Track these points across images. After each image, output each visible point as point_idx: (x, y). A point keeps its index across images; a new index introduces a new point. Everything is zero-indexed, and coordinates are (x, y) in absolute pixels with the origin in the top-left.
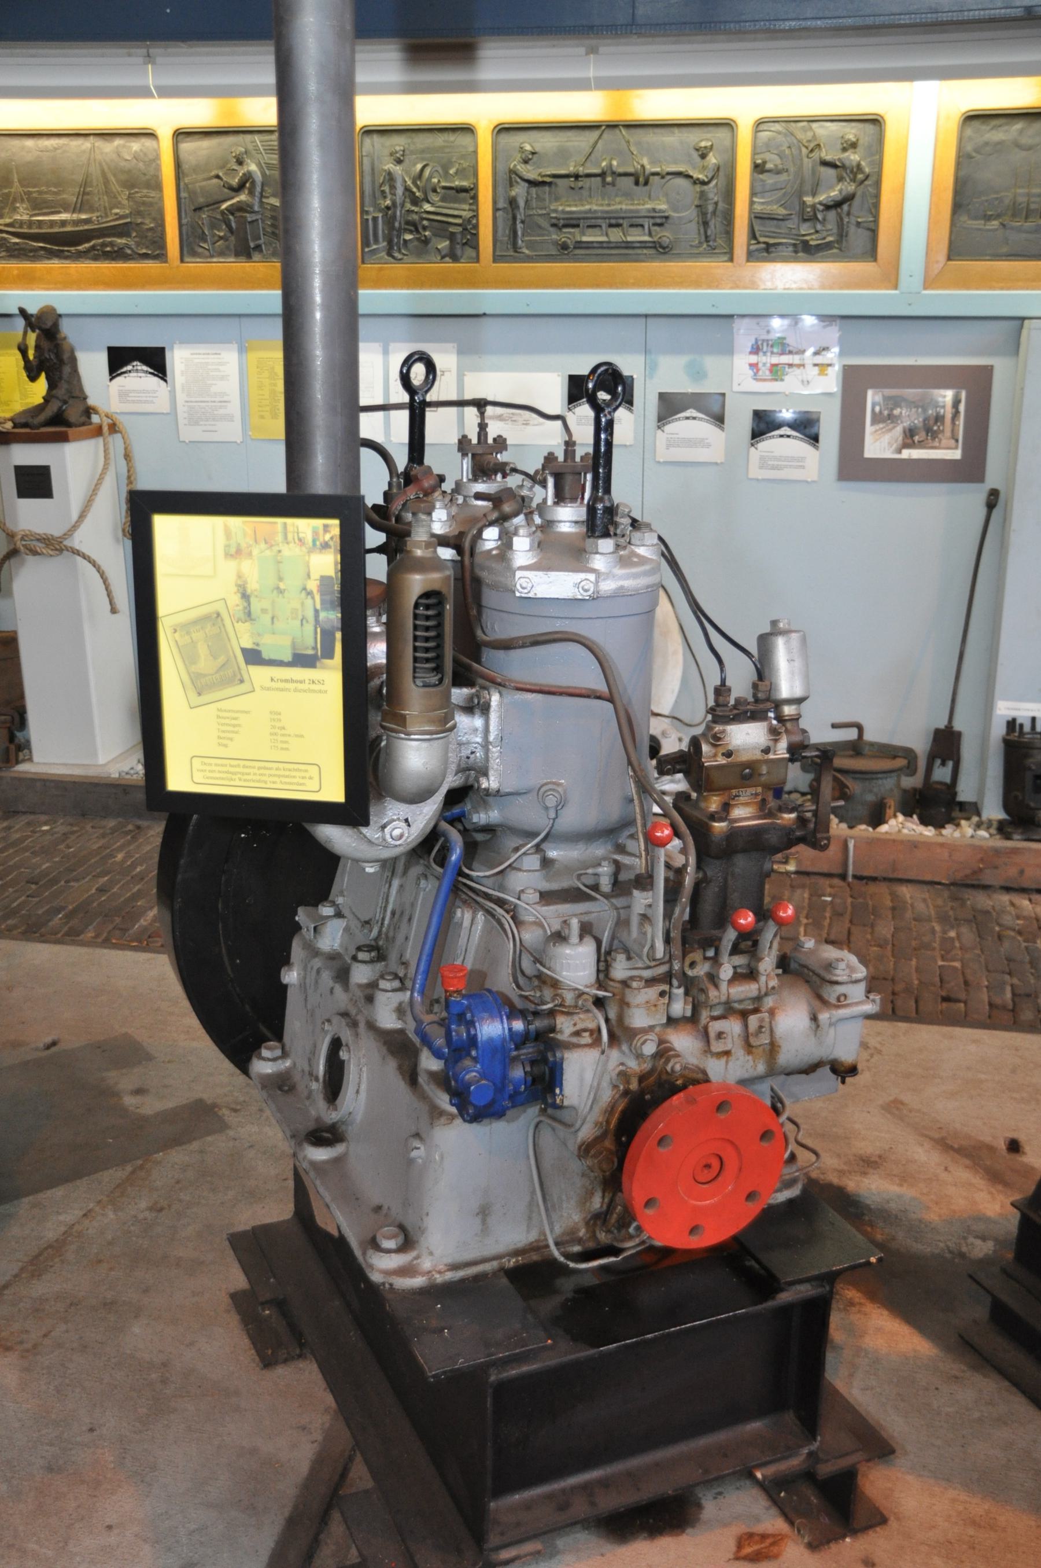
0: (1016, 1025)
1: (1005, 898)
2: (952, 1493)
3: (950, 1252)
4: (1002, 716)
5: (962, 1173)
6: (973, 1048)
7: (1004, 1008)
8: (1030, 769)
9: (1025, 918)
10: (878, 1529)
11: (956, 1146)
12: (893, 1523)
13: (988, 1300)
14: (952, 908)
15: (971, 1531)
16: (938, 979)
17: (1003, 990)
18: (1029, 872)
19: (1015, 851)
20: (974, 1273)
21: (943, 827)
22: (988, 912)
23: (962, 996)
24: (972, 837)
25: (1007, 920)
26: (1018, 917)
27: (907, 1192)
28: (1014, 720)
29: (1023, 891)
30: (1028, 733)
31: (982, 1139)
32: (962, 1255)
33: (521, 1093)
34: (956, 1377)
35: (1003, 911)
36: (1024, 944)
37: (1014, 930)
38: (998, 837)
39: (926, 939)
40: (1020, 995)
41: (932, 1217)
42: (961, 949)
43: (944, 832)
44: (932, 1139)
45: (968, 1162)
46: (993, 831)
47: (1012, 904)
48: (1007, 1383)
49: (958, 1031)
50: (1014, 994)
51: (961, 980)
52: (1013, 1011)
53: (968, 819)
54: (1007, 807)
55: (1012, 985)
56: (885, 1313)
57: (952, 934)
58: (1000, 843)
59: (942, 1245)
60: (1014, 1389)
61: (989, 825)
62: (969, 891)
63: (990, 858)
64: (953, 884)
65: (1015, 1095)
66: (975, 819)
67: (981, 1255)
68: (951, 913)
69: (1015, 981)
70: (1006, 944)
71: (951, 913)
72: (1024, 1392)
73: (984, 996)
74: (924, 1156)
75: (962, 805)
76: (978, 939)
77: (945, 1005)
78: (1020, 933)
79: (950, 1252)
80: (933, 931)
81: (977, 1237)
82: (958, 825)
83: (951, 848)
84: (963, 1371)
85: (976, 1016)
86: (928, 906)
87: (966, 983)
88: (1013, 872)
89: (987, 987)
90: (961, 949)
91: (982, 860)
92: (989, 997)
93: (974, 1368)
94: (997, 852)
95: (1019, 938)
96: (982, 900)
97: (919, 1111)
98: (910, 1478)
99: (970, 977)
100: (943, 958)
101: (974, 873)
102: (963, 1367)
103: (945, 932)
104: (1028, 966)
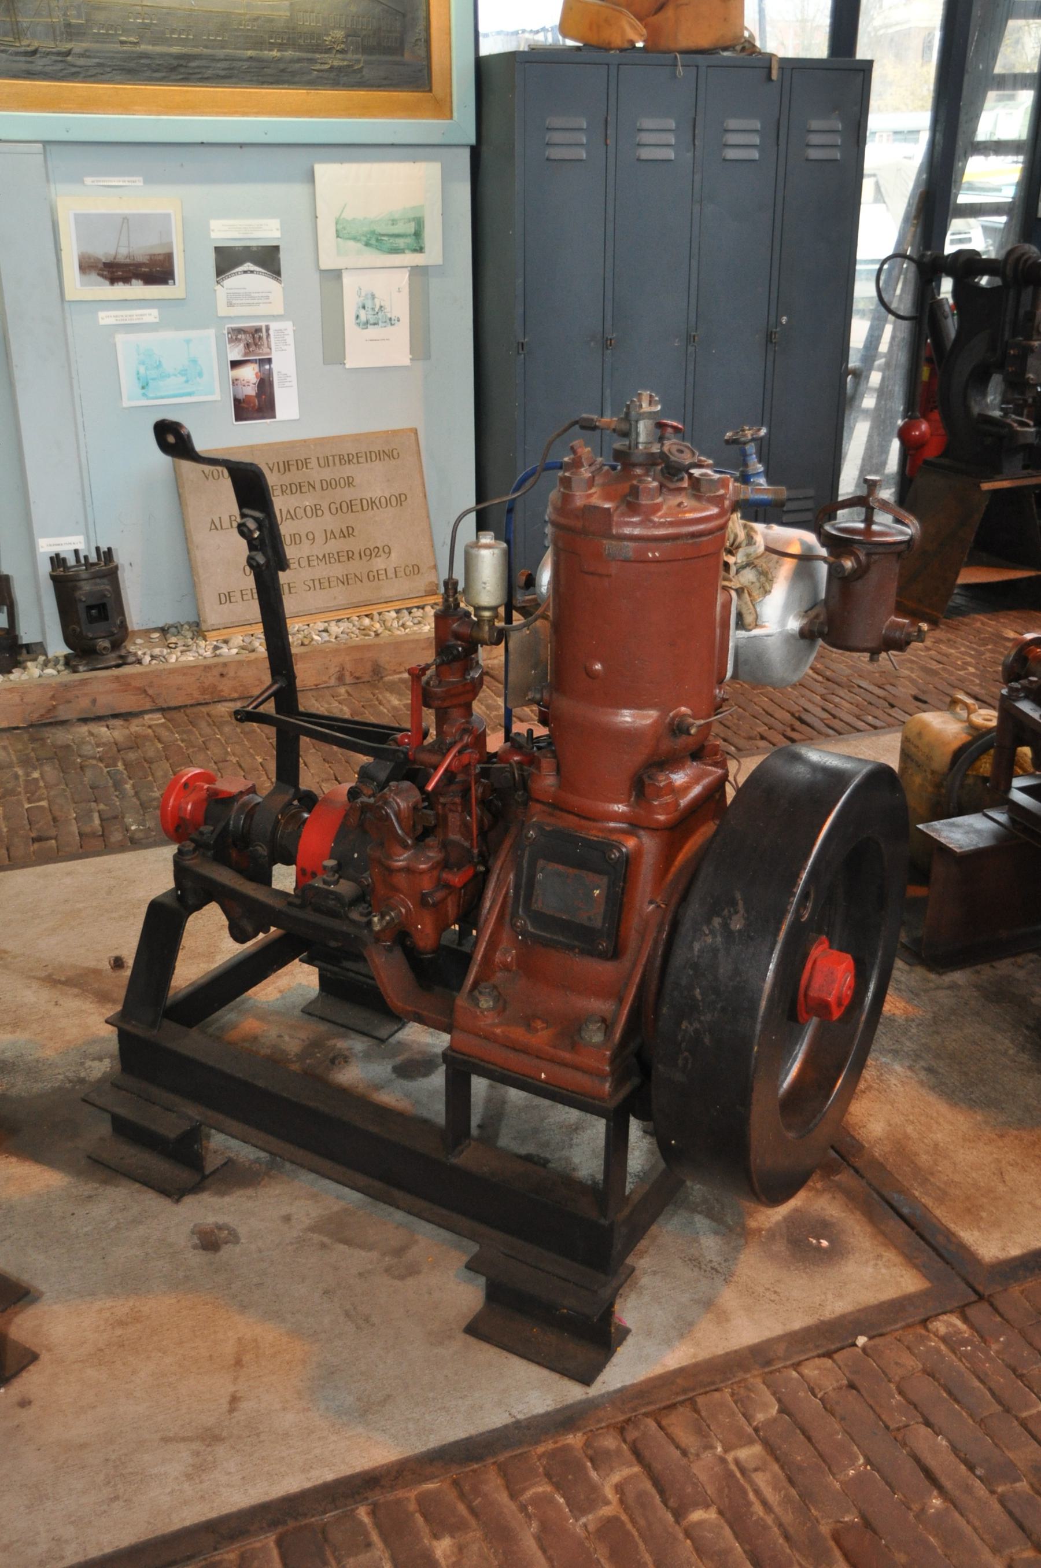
0: (108, 848)
1: (84, 729)
2: (98, 1305)
3: (70, 1081)
4: (44, 553)
5: (72, 1003)
6: (68, 881)
7: (94, 835)
8: (81, 600)
9: (104, 744)
10: (31, 1368)
11: (63, 979)
12: (45, 1357)
13: (107, 1117)
14: (33, 749)
15: (119, 1332)
16: (26, 822)
17: (91, 819)
18: (102, 700)
19: (83, 682)
20: (85, 1096)
21: (10, 672)
22: (68, 746)
23: (53, 832)
24: (40, 676)
25: (87, 750)
26: (98, 746)
27: (21, 1037)
28: (57, 555)
29: (98, 719)
30: (74, 567)
31: (86, 965)
32: (82, 1081)
33: (689, 734)
34: (90, 1197)
35: (83, 742)
36: (106, 770)
37: (94, 758)
38: (66, 672)
39: (9, 786)
40: (108, 819)
41: (49, 1053)
42: (46, 787)
43: (12, 677)
44: (38, 979)
45: (76, 991)
46: (60, 667)
47: (91, 734)
48: (137, 1185)
49: (51, 868)
50: (102, 820)
51: (50, 818)
52: (103, 835)
53: (35, 660)
54: (68, 642)
55: (99, 812)
56: (14, 1160)
57: (36, 775)
58: (67, 676)
59: (61, 1077)
60: (145, 1188)
61: (57, 660)
62: (48, 729)
63: (61, 693)
64: (31, 726)
65: (114, 915)
66: (41, 658)
67: (99, 1075)
68: (32, 754)
69: (102, 806)
70: (89, 773)
71: (32, 754)
72: (152, 1188)
73: (74, 829)
74: (34, 997)
75: (28, 647)
76: (61, 775)
77: (36, 845)
78: (101, 760)
79: (70, 1081)
80: (16, 777)
81: (94, 1059)
82: (25, 668)
83: (21, 690)
84: (97, 1189)
85: (67, 849)
86: (9, 754)
87: (55, 820)
88: (84, 703)
89: (75, 819)
90: (46, 787)
91: (53, 697)
92: (79, 828)
93: (105, 1182)
94: (66, 687)
95: (101, 765)
96: (61, 736)
97: (23, 954)
98: (55, 1307)
99: (57, 814)
100: (29, 801)
101: (49, 711)
102: (96, 1185)
103: (28, 775)
104: (112, 789)
